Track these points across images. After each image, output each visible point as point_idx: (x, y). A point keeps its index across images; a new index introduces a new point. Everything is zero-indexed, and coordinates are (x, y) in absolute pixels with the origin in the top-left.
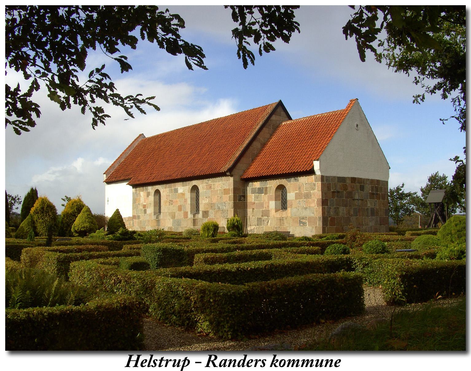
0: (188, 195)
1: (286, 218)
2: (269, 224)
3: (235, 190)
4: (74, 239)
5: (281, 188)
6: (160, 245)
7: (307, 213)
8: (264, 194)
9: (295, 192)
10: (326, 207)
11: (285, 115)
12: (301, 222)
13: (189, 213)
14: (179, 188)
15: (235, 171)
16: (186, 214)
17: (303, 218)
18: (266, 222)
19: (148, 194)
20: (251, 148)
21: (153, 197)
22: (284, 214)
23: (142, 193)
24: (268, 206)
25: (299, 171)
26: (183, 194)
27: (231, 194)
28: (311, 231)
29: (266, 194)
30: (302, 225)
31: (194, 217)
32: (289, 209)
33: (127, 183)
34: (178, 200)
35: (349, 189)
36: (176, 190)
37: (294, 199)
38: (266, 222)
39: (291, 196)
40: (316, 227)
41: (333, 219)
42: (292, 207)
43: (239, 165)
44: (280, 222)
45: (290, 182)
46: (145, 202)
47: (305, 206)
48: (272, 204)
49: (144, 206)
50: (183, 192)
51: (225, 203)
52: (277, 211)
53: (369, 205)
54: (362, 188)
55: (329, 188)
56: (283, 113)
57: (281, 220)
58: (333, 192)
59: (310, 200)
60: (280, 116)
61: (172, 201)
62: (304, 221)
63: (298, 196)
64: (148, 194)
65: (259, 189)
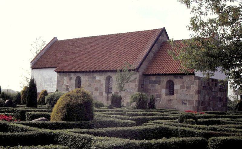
0: (104, 82)
1: (173, 100)
2: (161, 103)
3: (140, 81)
4: (104, 107)
5: (170, 81)
6: (36, 109)
7: (188, 98)
8: (158, 85)
9: (181, 85)
10: (200, 95)
11: (166, 37)
12: (183, 102)
13: (104, 93)
14: (96, 77)
15: (140, 70)
16: (101, 94)
17: (185, 101)
18: (158, 101)
19: (71, 79)
20: (149, 56)
21: (75, 81)
22: (172, 97)
23: (66, 79)
24: (161, 92)
25: (175, 73)
26: (99, 81)
27: (137, 83)
28: (190, 109)
29: (159, 84)
30: (184, 104)
31: (108, 95)
32: (175, 95)
33: (54, 70)
34: (95, 84)
35: (211, 85)
36: (94, 78)
37: (179, 89)
38: (158, 101)
39: (177, 87)
40: (193, 106)
41: (203, 102)
42: (177, 93)
43: (142, 66)
44: (169, 102)
45: (177, 78)
46: (68, 84)
47: (186, 94)
48: (164, 91)
49: (67, 86)
50: (100, 79)
51: (132, 88)
52: (167, 95)
53: (219, 95)
54: (216, 85)
55: (201, 84)
56: (165, 35)
57: (169, 101)
58: (203, 87)
59: (190, 90)
60: (163, 37)
61: (91, 84)
62: (185, 102)
63: (182, 87)
64: (71, 79)
65: (155, 81)
